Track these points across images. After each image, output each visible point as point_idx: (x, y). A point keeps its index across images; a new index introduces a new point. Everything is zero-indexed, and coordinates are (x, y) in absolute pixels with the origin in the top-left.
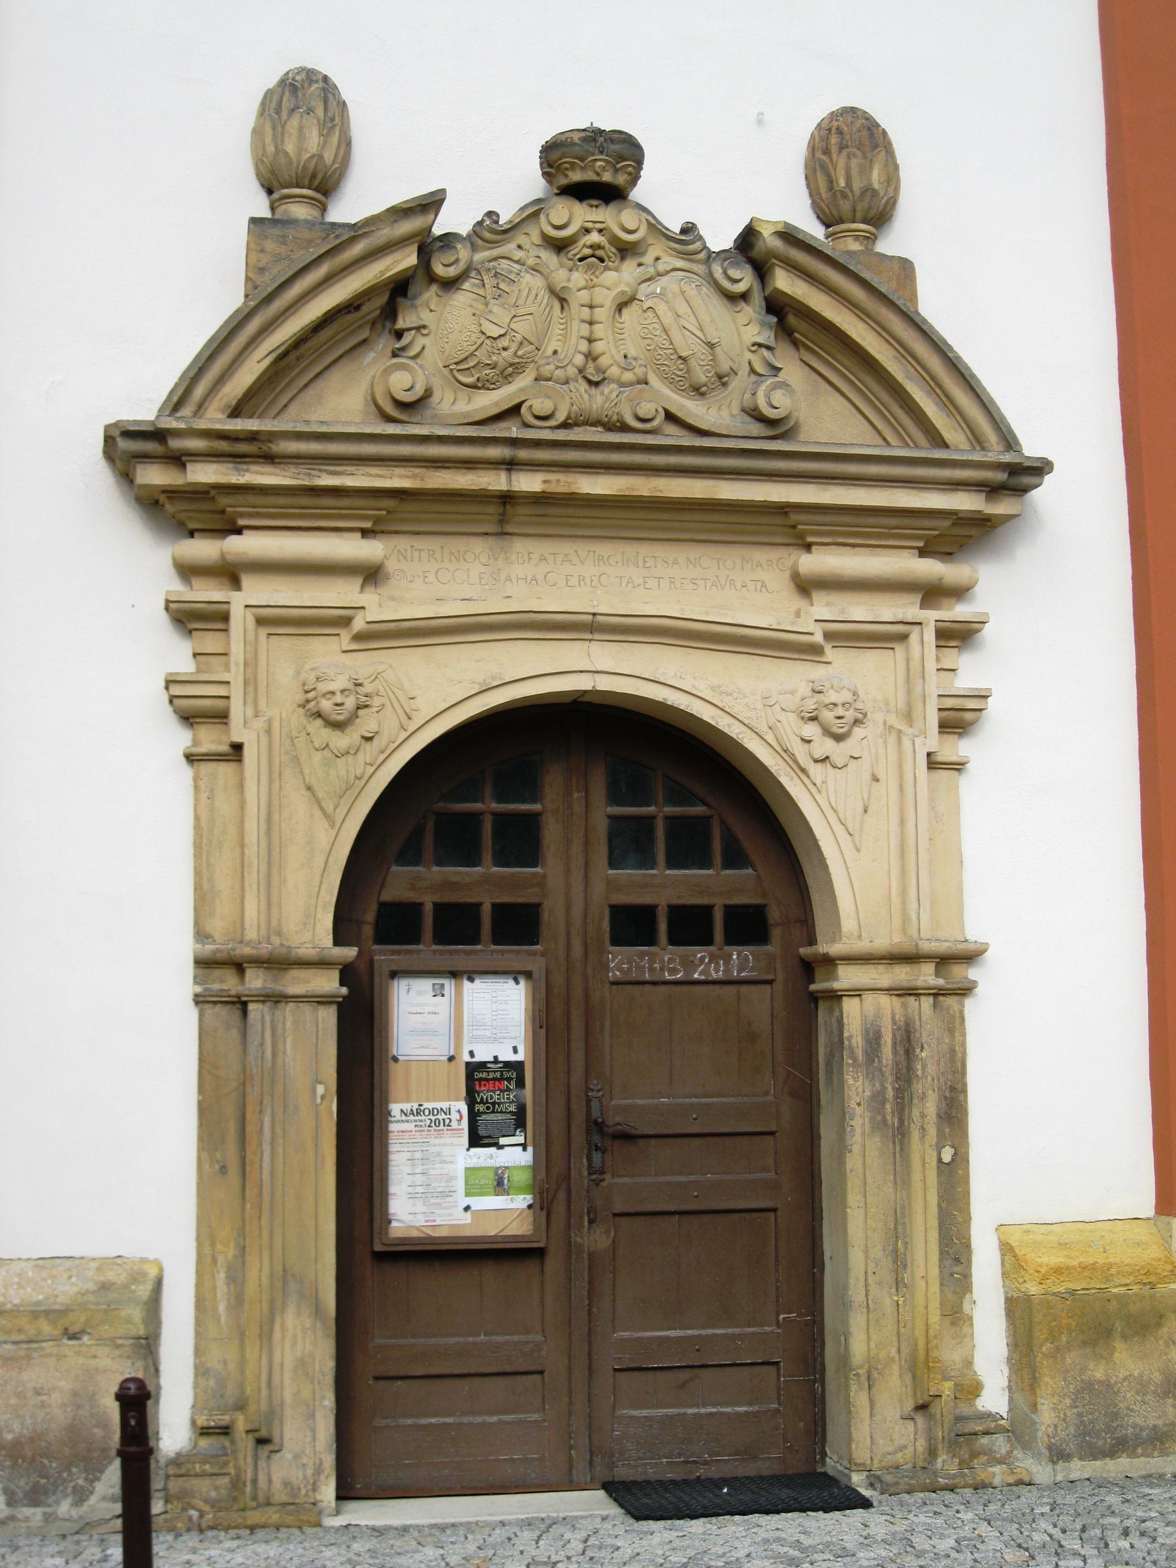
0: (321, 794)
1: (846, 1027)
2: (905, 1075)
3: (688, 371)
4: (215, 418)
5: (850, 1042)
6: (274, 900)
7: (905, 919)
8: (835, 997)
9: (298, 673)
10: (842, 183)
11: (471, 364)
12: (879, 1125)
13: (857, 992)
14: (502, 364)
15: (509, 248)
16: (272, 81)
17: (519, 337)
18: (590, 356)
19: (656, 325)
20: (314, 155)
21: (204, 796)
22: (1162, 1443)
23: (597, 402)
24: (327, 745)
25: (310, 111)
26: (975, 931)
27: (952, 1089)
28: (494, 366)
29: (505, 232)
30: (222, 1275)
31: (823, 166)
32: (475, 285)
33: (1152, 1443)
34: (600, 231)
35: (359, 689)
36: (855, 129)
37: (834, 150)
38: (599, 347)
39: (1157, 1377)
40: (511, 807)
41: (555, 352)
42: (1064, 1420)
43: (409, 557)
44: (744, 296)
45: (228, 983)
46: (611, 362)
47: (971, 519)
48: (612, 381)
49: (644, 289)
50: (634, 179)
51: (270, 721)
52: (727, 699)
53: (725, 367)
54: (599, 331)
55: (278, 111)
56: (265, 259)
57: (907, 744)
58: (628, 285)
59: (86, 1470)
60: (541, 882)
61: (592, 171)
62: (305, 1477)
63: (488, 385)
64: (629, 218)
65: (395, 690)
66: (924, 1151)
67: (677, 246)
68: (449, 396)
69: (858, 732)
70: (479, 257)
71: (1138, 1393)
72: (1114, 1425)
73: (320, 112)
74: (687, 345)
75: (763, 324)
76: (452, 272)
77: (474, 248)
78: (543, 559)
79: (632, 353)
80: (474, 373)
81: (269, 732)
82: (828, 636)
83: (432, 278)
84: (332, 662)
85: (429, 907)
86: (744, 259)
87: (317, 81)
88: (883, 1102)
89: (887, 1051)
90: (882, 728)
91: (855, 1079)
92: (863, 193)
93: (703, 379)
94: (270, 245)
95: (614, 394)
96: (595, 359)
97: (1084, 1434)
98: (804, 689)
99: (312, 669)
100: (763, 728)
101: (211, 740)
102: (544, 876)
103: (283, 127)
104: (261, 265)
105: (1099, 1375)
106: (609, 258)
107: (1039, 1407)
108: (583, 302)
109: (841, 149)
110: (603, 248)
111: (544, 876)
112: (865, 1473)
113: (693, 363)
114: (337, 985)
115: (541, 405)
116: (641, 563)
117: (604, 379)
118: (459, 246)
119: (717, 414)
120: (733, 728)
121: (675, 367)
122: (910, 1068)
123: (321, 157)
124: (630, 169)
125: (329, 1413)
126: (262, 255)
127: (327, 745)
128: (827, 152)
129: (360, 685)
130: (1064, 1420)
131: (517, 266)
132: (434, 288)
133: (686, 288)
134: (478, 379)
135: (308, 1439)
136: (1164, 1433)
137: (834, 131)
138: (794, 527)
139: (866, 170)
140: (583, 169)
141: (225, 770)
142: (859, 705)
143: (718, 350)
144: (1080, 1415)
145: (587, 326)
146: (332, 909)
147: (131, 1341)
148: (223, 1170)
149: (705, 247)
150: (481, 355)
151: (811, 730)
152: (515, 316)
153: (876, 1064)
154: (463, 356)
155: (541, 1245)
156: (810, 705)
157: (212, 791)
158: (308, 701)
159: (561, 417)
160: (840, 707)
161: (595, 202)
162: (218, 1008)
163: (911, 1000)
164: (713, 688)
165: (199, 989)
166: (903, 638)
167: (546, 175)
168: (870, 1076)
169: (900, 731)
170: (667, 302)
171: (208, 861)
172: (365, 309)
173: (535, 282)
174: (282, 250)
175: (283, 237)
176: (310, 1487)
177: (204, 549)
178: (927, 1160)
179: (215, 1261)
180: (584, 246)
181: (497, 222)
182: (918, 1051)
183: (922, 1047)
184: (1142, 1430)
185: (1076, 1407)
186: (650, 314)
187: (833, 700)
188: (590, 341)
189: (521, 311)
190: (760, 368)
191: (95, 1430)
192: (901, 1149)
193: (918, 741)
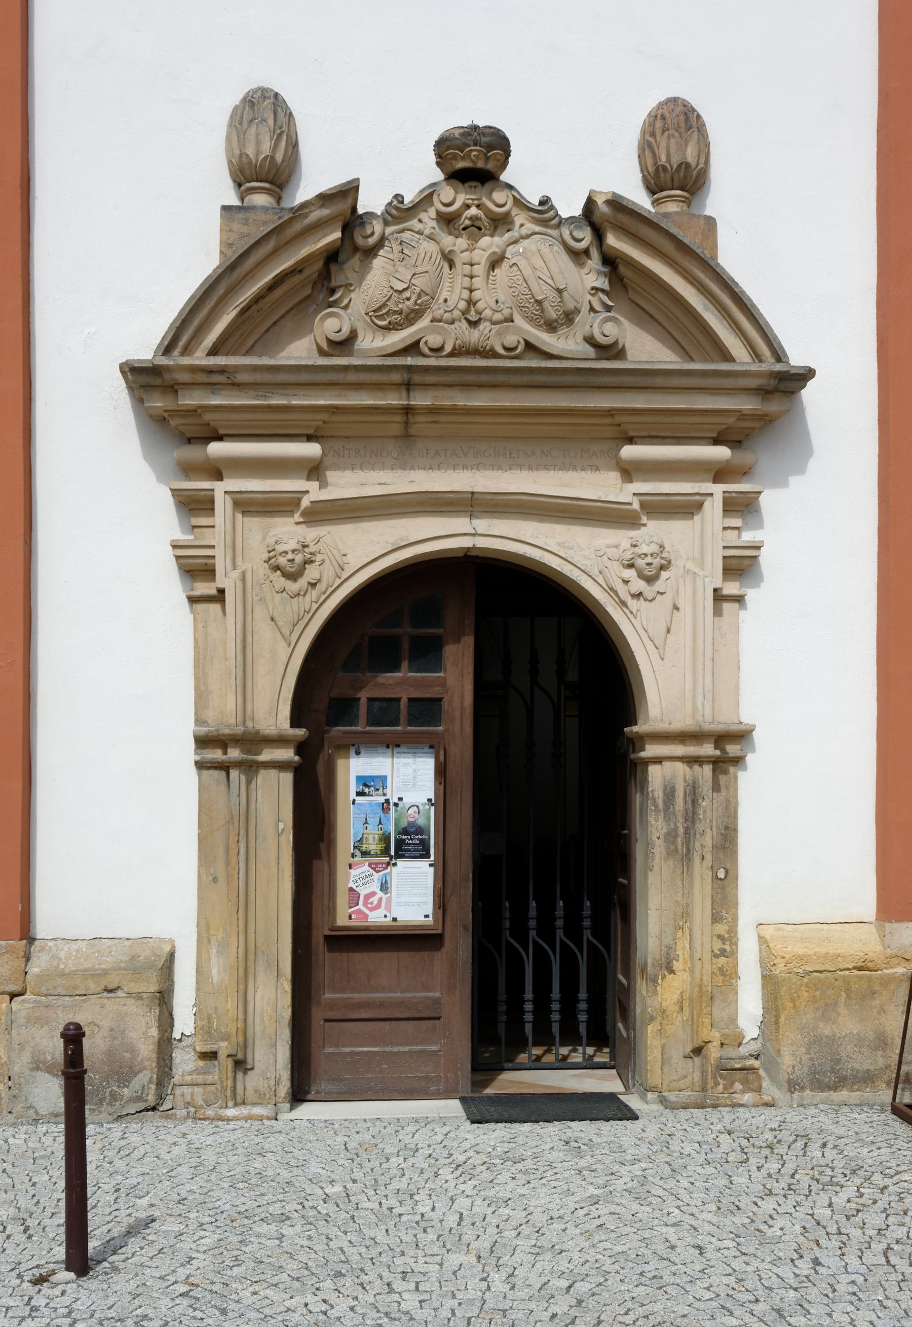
0: (280, 623)
2: (691, 817)
3: (542, 311)
4: (200, 358)
5: (653, 794)
6: (249, 696)
7: (695, 709)
8: (647, 762)
9: (264, 538)
10: (664, 158)
12: (671, 852)
13: (659, 760)
14: (405, 309)
15: (414, 223)
16: (237, 99)
17: (418, 290)
18: (471, 303)
19: (519, 277)
20: (267, 156)
21: (200, 628)
22: (873, 1082)
23: (474, 337)
24: (284, 589)
25: (264, 120)
26: (747, 716)
27: (726, 828)
28: (400, 312)
29: (409, 209)
31: (650, 146)
32: (387, 251)
33: (865, 1082)
34: (478, 206)
35: (306, 550)
36: (674, 115)
37: (658, 133)
38: (477, 295)
39: (871, 1035)
40: (422, 631)
41: (446, 301)
44: (586, 252)
45: (216, 755)
46: (486, 306)
47: (752, 415)
48: (486, 320)
49: (510, 250)
50: (504, 164)
51: (244, 574)
53: (571, 305)
54: (477, 282)
56: (233, 237)
57: (699, 582)
58: (498, 247)
59: (118, 1081)
60: (443, 683)
61: (474, 159)
62: (269, 1087)
64: (499, 196)
65: (332, 550)
67: (535, 215)
68: (369, 337)
69: (664, 574)
70: (389, 230)
71: (856, 1046)
72: (837, 1067)
73: (271, 122)
74: (542, 291)
75: (599, 273)
76: (371, 241)
77: (386, 223)
78: (437, 453)
79: (501, 298)
80: (388, 318)
81: (243, 580)
82: (643, 505)
83: (356, 249)
84: (287, 532)
86: (587, 223)
87: (269, 98)
90: (682, 571)
92: (680, 166)
93: (554, 316)
94: (236, 226)
95: (487, 331)
96: (474, 304)
97: (815, 1073)
98: (626, 544)
99: (274, 536)
100: (595, 572)
101: (204, 588)
102: (444, 679)
103: (244, 134)
104: (230, 241)
105: (827, 1031)
106: (485, 227)
108: (466, 261)
109: (663, 131)
110: (480, 219)
112: (657, 1094)
113: (546, 305)
114: (292, 755)
115: (434, 340)
116: (508, 456)
117: (480, 319)
118: (374, 222)
119: (567, 344)
120: (574, 572)
121: (533, 309)
122: (694, 813)
123: (273, 158)
124: (498, 157)
125: (286, 1043)
126: (230, 234)
127: (284, 589)
128: (653, 134)
129: (307, 546)
131: (417, 236)
132: (358, 256)
133: (542, 247)
134: (390, 322)
135: (273, 1059)
136: (874, 1075)
137: (659, 117)
138: (619, 425)
139: (682, 148)
140: (463, 158)
141: (215, 607)
142: (665, 555)
143: (565, 294)
145: (469, 279)
146: (290, 702)
147: (698, 980)
148: (215, 880)
149: (557, 215)
150: (391, 305)
151: (630, 574)
152: (414, 274)
153: (671, 810)
154: (378, 305)
156: (628, 555)
157: (206, 622)
158: (270, 559)
159: (448, 349)
160: (649, 556)
161: (473, 184)
162: (210, 772)
163: (696, 767)
164: (559, 545)
165: (198, 758)
166: (700, 506)
167: (438, 164)
168: (667, 819)
169: (695, 573)
170: (527, 258)
172: (307, 272)
173: (431, 248)
174: (245, 229)
175: (246, 219)
176: (272, 1093)
177: (192, 453)
179: (209, 941)
180: (466, 218)
181: (402, 202)
182: (700, 801)
184: (858, 1072)
186: (515, 268)
187: (644, 551)
188: (471, 291)
189: (419, 270)
190: (597, 307)
191: (125, 1054)
192: (688, 869)
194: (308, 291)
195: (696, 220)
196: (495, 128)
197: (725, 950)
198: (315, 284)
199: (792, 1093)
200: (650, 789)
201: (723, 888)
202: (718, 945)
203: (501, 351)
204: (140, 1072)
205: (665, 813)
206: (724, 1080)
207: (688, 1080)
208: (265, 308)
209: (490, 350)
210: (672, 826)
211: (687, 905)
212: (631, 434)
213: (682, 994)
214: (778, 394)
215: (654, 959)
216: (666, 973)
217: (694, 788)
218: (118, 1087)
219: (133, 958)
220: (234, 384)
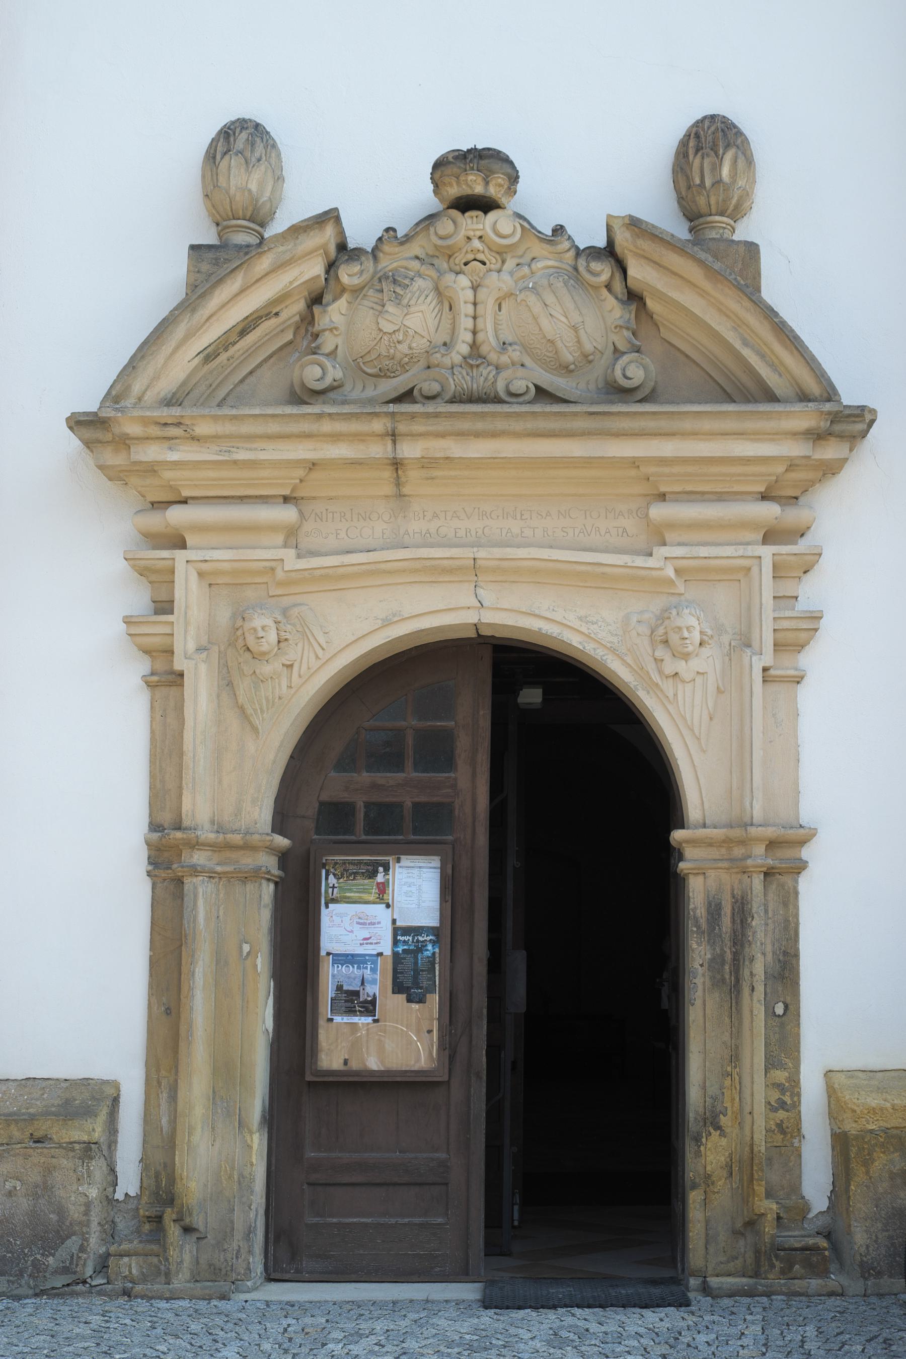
1: (692, 900)
2: (740, 940)
11: (373, 357)
12: (717, 982)
27: (785, 953)
30: (165, 1095)
42: (876, 1241)
43: (324, 520)
50: (511, 191)
52: (592, 627)
55: (214, 158)
61: (472, 182)
62: (226, 1260)
63: (389, 374)
66: (755, 1008)
85: (360, 805)
88: (723, 963)
89: (726, 921)
90: (728, 647)
91: (699, 944)
94: (205, 267)
103: (217, 168)
107: (853, 1229)
111: (456, 779)
126: (198, 275)
128: (686, 155)
130: (876, 1241)
137: (692, 136)
144: (890, 1238)
147: (748, 1139)
153: (717, 931)
155: (446, 1078)
157: (165, 710)
164: (580, 619)
168: (712, 943)
171: (161, 766)
175: (216, 259)
176: (229, 1268)
177: (155, 521)
178: (755, 1012)
179: (159, 1083)
182: (749, 920)
183: (753, 917)
185: (887, 1231)
191: (51, 1216)
192: (737, 1003)
193: (754, 658)
194: (289, 336)
195: (735, 247)
196: (495, 150)
197: (785, 1103)
198: (297, 328)
199: (866, 1279)
200: (691, 906)
201: (782, 1025)
202: (775, 1095)
203: (503, 395)
204: (68, 1237)
205: (709, 935)
206: (781, 1262)
207: (739, 1263)
208: (236, 356)
209: (495, 397)
210: (718, 951)
211: (737, 1047)
212: (663, 489)
213: (731, 1155)
214: (833, 439)
215: (697, 1112)
216: (712, 1131)
217: (742, 903)
218: (43, 1255)
219: (67, 1102)
220: (193, 438)
